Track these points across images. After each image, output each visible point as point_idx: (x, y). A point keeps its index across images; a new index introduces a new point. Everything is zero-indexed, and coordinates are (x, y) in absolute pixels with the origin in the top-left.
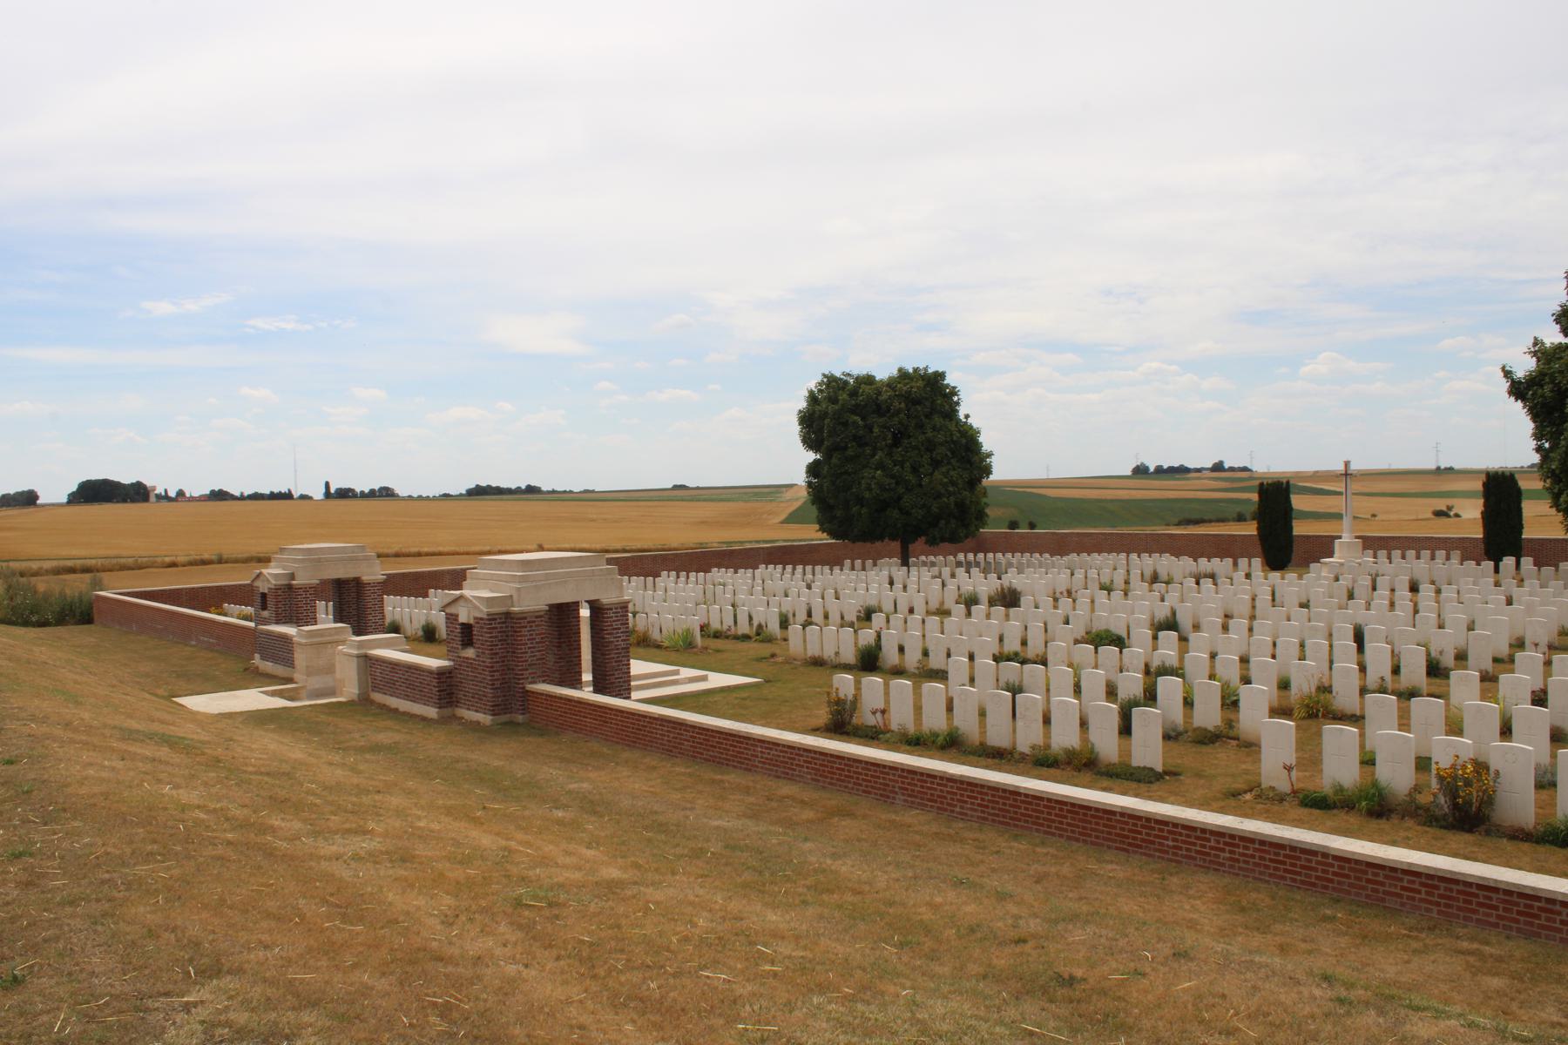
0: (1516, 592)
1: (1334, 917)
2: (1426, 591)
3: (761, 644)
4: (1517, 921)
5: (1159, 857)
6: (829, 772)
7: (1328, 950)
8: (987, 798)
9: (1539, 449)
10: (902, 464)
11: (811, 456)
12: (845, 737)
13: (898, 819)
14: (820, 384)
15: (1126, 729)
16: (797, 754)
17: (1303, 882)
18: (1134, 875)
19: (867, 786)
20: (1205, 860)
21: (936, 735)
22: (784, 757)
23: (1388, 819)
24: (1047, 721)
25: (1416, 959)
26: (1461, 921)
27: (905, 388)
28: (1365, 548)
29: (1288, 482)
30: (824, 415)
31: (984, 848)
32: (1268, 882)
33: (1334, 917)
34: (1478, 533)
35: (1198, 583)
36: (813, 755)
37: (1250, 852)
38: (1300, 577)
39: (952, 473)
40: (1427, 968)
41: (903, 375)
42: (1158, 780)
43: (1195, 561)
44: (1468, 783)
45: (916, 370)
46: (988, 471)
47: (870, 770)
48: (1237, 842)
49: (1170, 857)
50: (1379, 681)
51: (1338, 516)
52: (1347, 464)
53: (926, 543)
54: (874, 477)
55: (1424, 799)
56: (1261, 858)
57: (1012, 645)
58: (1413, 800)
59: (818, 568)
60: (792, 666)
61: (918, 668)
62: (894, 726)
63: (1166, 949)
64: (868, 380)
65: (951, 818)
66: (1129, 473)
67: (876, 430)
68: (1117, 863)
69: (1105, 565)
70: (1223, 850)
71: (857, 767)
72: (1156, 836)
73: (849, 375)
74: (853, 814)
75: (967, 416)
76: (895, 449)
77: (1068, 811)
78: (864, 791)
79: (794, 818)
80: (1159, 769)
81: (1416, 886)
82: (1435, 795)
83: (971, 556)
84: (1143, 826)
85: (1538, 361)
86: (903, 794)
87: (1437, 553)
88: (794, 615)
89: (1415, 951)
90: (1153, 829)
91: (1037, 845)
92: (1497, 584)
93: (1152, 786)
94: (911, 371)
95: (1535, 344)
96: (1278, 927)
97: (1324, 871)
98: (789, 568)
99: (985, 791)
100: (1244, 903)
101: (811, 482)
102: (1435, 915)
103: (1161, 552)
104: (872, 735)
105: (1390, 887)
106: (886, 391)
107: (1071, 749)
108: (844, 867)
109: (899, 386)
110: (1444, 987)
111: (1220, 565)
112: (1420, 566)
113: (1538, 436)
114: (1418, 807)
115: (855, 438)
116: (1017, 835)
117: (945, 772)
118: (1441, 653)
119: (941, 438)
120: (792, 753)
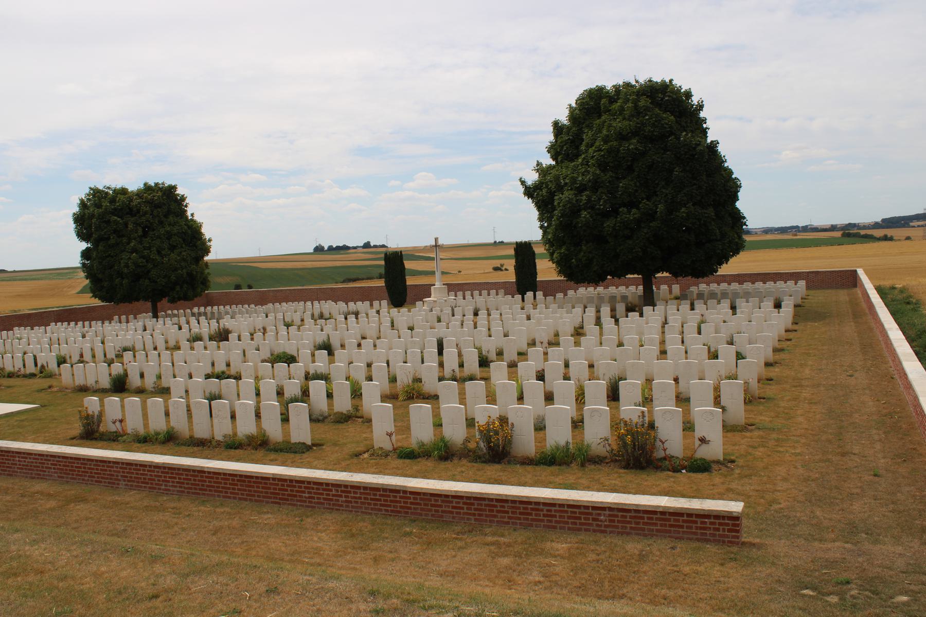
0: (532, 312)
1: (411, 532)
2: (483, 314)
3: (44, 380)
4: (519, 519)
5: (300, 505)
6: (70, 470)
7: (405, 556)
8: (182, 477)
9: (542, 227)
10: (149, 248)
11: (84, 245)
12: (94, 442)
13: (120, 499)
14: (88, 195)
15: (285, 419)
16: (45, 460)
17: (392, 511)
18: (282, 520)
19: (98, 477)
20: (330, 504)
21: (157, 434)
22: (36, 463)
23: (451, 461)
24: (233, 417)
25: (459, 554)
26: (488, 523)
27: (149, 197)
28: (449, 291)
29: (401, 252)
30: (92, 216)
31: (180, 513)
32: (370, 514)
33: (411, 532)
34: (513, 279)
35: (346, 318)
36: (57, 459)
37: (358, 495)
38: (409, 311)
40: (466, 558)
41: (147, 188)
42: (308, 450)
43: (347, 304)
44: (497, 433)
45: (157, 184)
46: (207, 251)
47: (99, 466)
48: (349, 489)
49: (307, 504)
50: (452, 372)
51: (433, 273)
52: (436, 239)
53: (168, 302)
54: (130, 258)
55: (472, 445)
56: (365, 498)
57: (220, 367)
58: (466, 447)
59: (93, 323)
60: (63, 393)
61: (154, 388)
62: (129, 431)
63: (262, 587)
64: (124, 191)
65: (158, 494)
66: (312, 251)
67: (131, 226)
68: (271, 513)
69: (292, 310)
70: (341, 496)
71: (90, 465)
72: (297, 491)
73: (109, 188)
74: (86, 500)
76: (144, 239)
77: (238, 481)
78: (96, 481)
79: (39, 508)
80: (309, 443)
81: (461, 505)
82: (477, 443)
83: (202, 309)
84: (288, 486)
85: (540, 175)
86: (124, 481)
87: (483, 291)
88: (70, 357)
89: (460, 548)
90: (295, 486)
91: (217, 507)
92: (523, 308)
93: (303, 455)
94: (153, 185)
95: (538, 165)
96: (375, 544)
97: (405, 503)
98: (72, 324)
99: (181, 472)
100: (354, 531)
101: (85, 264)
102: (473, 522)
103: (326, 300)
104: (113, 439)
105: (445, 507)
106: (136, 199)
107: (250, 434)
108: (36, 552)
109: (145, 195)
110: (475, 570)
111: (362, 306)
112: (480, 300)
113: (541, 219)
114: (470, 451)
115: (115, 231)
116: (204, 501)
117: (152, 462)
118: (488, 352)
119: (175, 229)
120: (42, 459)
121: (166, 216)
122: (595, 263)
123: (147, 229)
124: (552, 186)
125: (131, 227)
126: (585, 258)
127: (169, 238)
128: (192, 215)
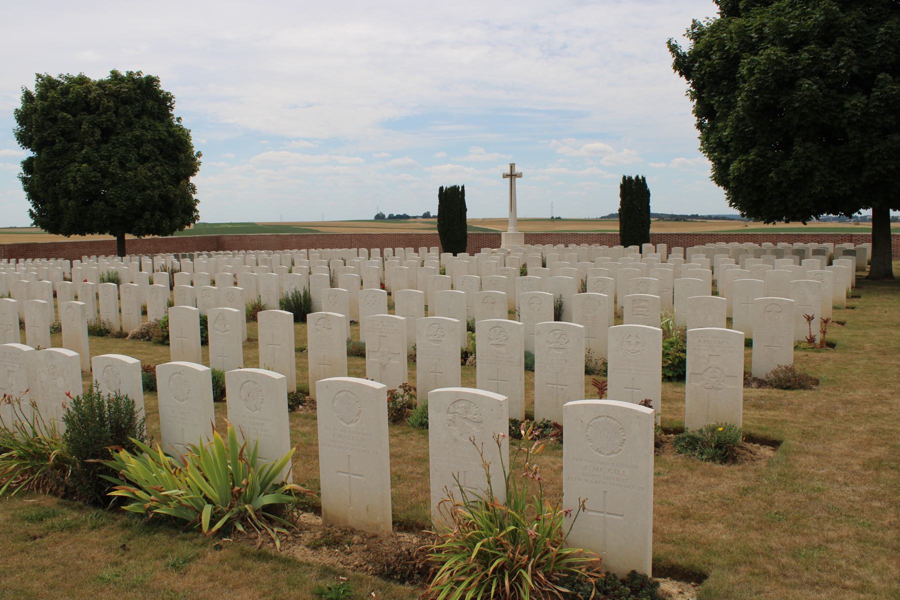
9: (700, 126)
10: (108, 159)
11: (28, 153)
27: (114, 88)
52: (512, 166)
54: (79, 170)
64: (82, 80)
67: (84, 126)
75: (179, 119)
95: (693, 27)
113: (699, 113)
115: (63, 133)
121: (138, 116)
122: (816, 180)
123: (107, 133)
124: (732, 46)
125: (85, 127)
126: (796, 170)
127: (138, 147)
128: (179, 119)
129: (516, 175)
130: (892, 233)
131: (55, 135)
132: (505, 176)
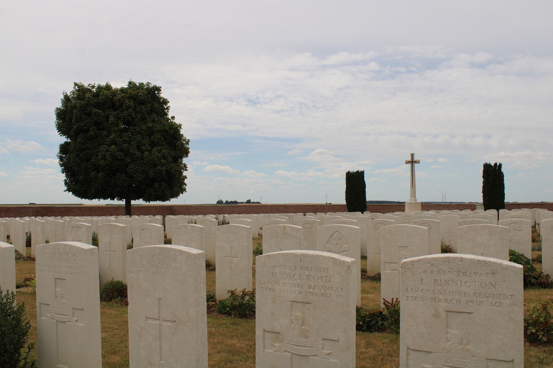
10: (129, 142)
11: (64, 139)
27: (133, 93)
39: (164, 151)
52: (412, 155)
75: (173, 118)
129: (416, 162)
130: (367, 204)
131: (89, 125)
132: (407, 162)
